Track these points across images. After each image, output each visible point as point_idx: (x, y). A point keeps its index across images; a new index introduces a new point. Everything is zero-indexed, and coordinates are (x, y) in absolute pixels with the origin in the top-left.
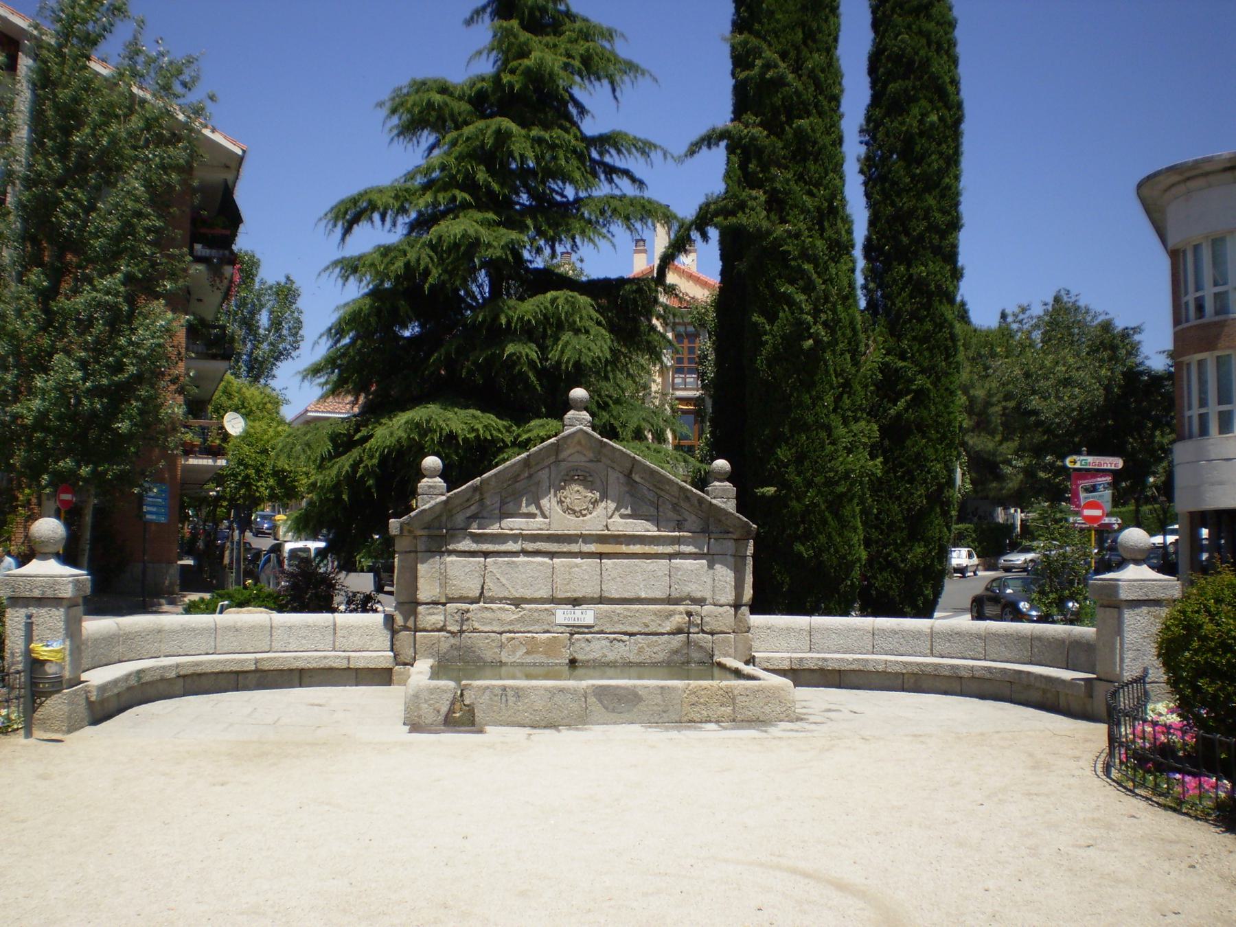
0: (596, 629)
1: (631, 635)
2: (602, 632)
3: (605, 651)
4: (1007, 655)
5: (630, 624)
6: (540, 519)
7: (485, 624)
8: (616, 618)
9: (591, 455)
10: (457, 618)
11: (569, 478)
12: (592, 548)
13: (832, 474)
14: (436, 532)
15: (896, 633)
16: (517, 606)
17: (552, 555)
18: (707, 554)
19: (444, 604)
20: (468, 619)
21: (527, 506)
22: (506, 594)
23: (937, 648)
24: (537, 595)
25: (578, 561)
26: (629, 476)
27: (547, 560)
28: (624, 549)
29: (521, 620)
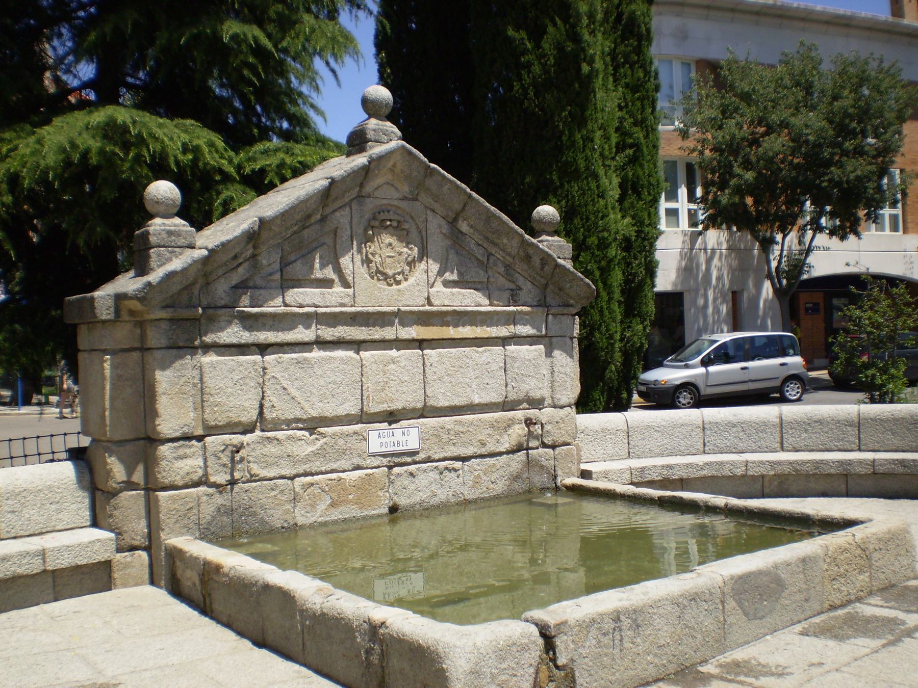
0: (421, 456)
1: (464, 459)
2: (429, 460)
3: (434, 487)
4: (896, 442)
5: (464, 444)
6: (338, 289)
7: (268, 465)
8: (445, 437)
9: (405, 189)
10: (225, 459)
11: (377, 223)
12: (412, 332)
13: (606, 234)
14: (186, 313)
15: (734, 426)
16: (311, 430)
17: (358, 345)
18: (546, 336)
19: (200, 439)
20: (242, 460)
21: (323, 266)
22: (298, 414)
23: (789, 440)
24: (341, 411)
25: (393, 353)
26: (453, 222)
27: (351, 354)
28: (452, 332)
29: (320, 454)
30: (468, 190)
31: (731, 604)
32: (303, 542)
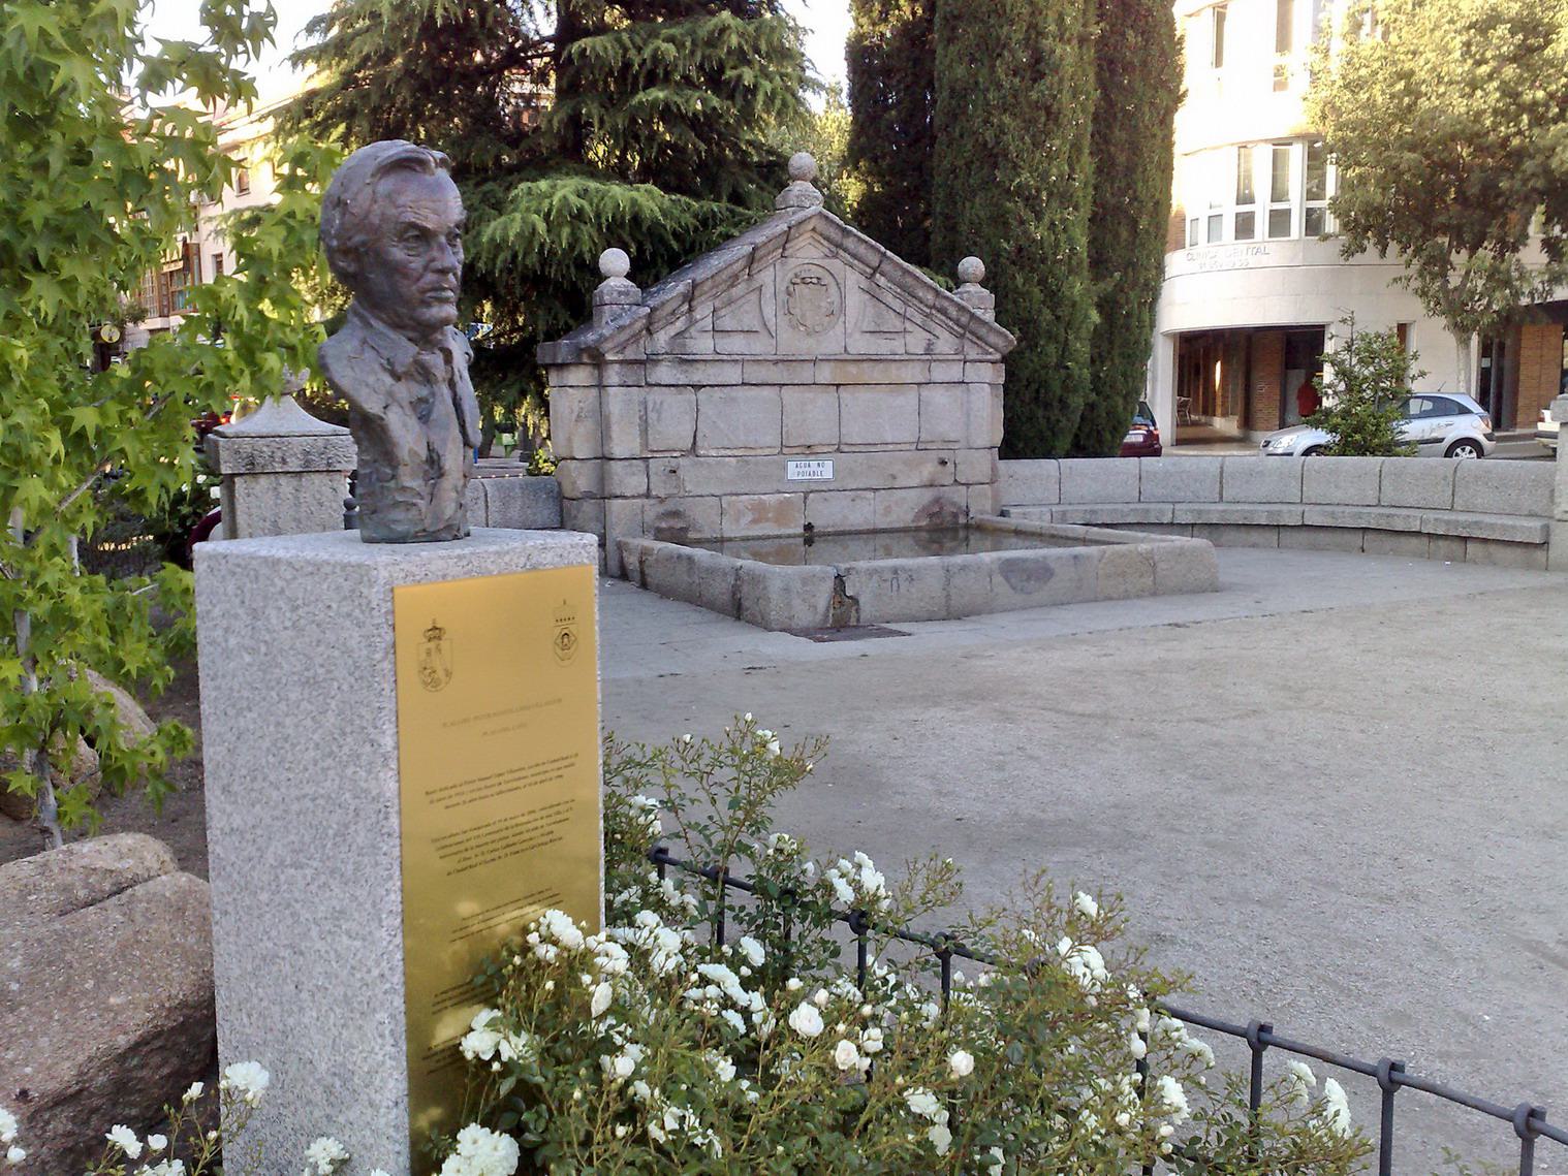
30: (883, 249)
31: (998, 579)
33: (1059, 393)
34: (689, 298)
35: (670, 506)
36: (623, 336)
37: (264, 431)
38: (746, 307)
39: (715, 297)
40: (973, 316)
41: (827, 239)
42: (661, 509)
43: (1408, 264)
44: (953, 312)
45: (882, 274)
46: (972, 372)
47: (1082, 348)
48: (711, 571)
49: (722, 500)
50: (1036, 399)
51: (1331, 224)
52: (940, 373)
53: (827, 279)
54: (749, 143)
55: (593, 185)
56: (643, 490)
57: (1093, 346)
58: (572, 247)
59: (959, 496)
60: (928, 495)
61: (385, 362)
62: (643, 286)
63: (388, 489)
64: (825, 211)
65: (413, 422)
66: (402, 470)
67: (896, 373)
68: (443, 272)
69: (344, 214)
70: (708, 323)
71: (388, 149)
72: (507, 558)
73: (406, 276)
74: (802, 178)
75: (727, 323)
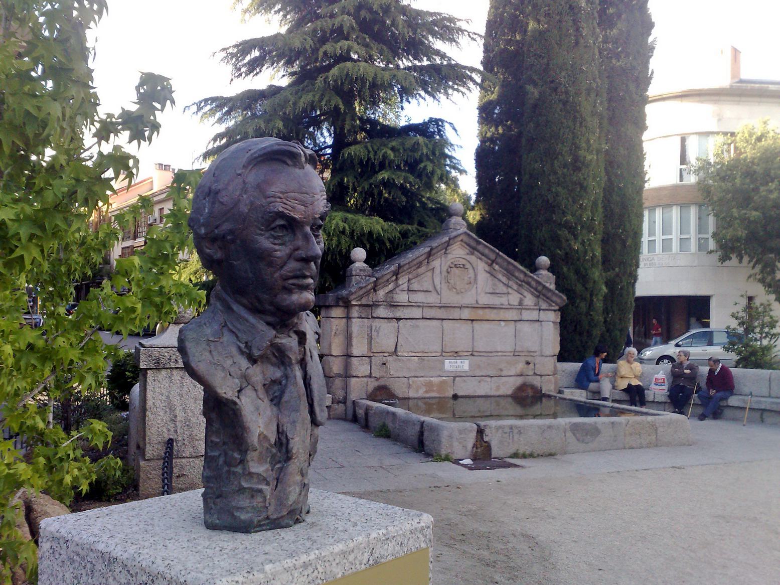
6: (434, 294)
30: (497, 251)
31: (569, 434)
32: (411, 403)
33: (587, 328)
34: (396, 274)
35: (382, 382)
36: (361, 292)
37: (167, 344)
38: (426, 279)
39: (410, 273)
40: (544, 287)
41: (468, 245)
42: (376, 384)
43: (753, 267)
44: (533, 283)
45: (497, 264)
46: (544, 316)
47: (599, 305)
48: (406, 422)
49: (411, 379)
50: (575, 330)
51: (712, 245)
52: (526, 315)
53: (468, 266)
54: (428, 198)
55: (350, 216)
56: (368, 373)
57: (605, 304)
58: (337, 246)
59: (536, 381)
60: (519, 381)
61: (243, 346)
62: (373, 266)
63: (234, 473)
64: (468, 232)
65: (265, 406)
66: (252, 455)
67: (503, 315)
68: (306, 260)
69: (213, 203)
70: (405, 286)
71: (262, 142)
72: (351, 558)
73: (270, 264)
74: (457, 215)
75: (415, 286)
